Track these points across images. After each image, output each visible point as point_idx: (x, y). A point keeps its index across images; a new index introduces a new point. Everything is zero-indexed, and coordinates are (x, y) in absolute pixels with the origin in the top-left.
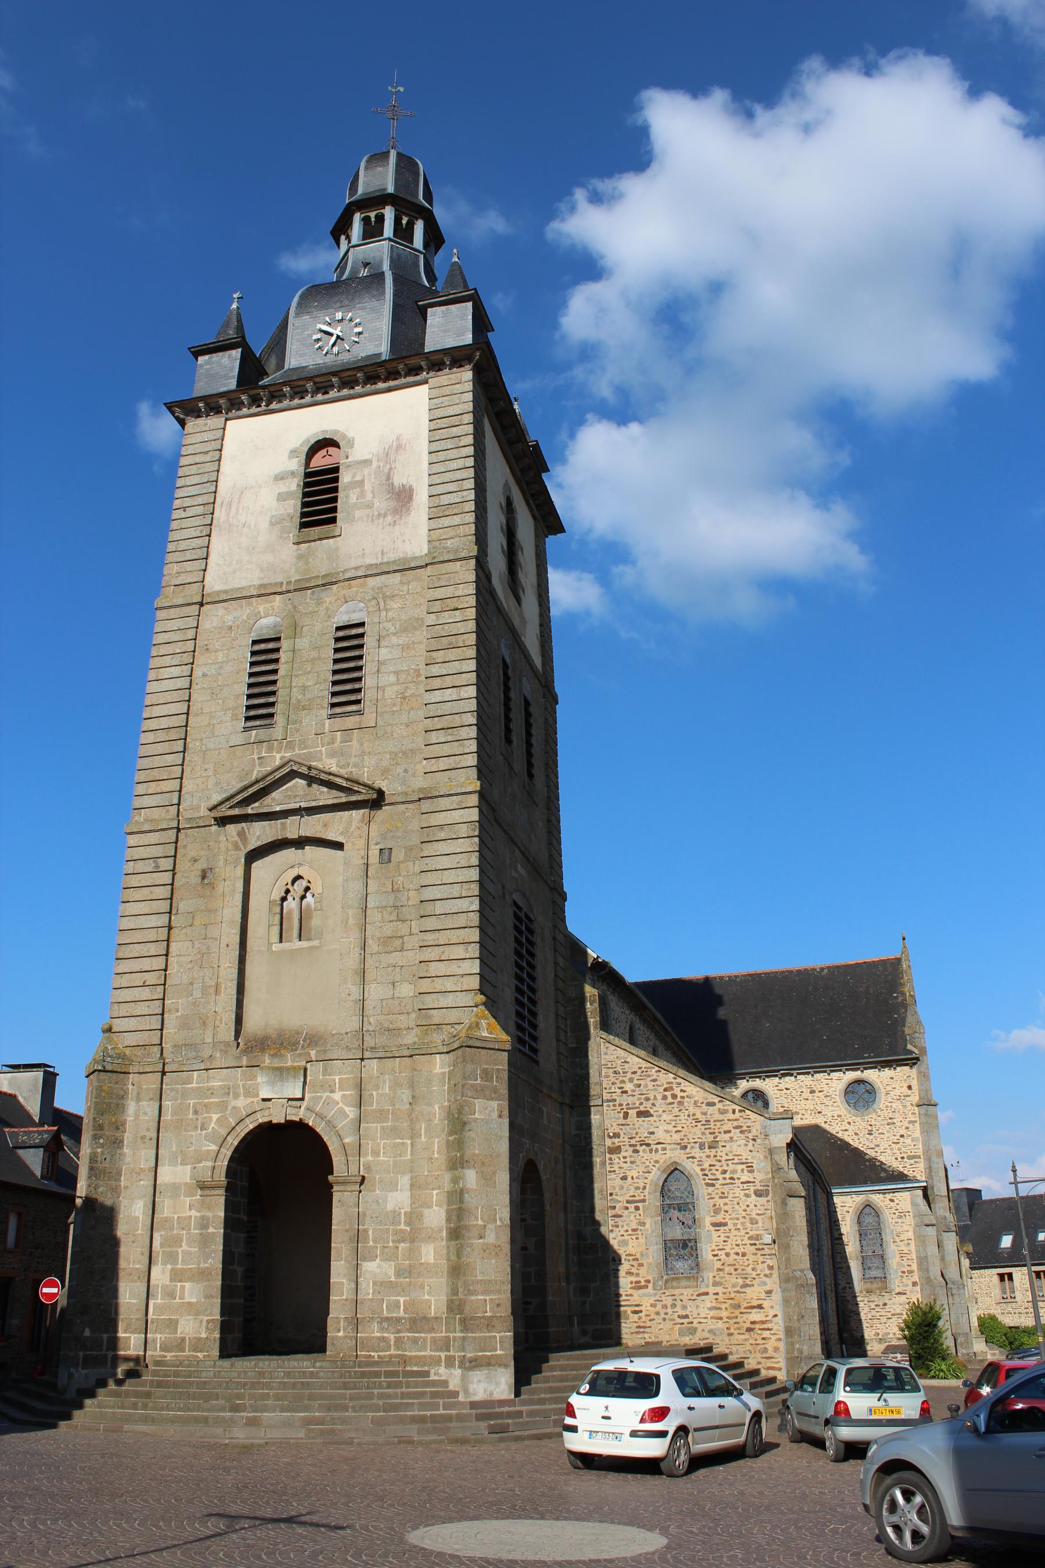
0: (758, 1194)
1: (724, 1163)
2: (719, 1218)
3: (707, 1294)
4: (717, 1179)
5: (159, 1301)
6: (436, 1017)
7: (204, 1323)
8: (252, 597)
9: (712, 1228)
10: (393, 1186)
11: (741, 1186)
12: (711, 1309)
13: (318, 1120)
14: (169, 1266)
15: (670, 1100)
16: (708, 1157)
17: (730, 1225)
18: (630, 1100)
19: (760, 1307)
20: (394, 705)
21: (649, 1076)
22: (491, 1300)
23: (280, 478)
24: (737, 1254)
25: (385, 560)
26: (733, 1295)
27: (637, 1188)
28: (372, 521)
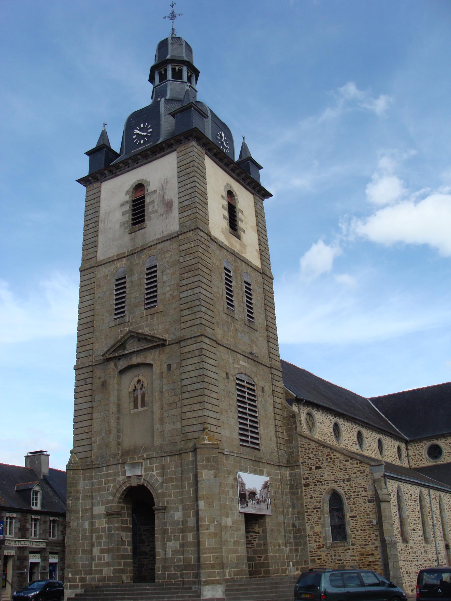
0: (370, 501)
1: (354, 488)
2: (353, 514)
3: (349, 549)
4: (351, 496)
5: (96, 562)
6: (190, 436)
7: (112, 570)
9: (350, 519)
10: (177, 509)
11: (362, 498)
12: (351, 556)
13: (148, 484)
14: (99, 548)
15: (329, 460)
16: (347, 485)
17: (358, 517)
19: (372, 554)
20: (169, 300)
21: (320, 450)
22: (213, 556)
23: (122, 205)
24: (362, 530)
25: (164, 236)
26: (360, 549)
27: (317, 502)
28: (158, 218)
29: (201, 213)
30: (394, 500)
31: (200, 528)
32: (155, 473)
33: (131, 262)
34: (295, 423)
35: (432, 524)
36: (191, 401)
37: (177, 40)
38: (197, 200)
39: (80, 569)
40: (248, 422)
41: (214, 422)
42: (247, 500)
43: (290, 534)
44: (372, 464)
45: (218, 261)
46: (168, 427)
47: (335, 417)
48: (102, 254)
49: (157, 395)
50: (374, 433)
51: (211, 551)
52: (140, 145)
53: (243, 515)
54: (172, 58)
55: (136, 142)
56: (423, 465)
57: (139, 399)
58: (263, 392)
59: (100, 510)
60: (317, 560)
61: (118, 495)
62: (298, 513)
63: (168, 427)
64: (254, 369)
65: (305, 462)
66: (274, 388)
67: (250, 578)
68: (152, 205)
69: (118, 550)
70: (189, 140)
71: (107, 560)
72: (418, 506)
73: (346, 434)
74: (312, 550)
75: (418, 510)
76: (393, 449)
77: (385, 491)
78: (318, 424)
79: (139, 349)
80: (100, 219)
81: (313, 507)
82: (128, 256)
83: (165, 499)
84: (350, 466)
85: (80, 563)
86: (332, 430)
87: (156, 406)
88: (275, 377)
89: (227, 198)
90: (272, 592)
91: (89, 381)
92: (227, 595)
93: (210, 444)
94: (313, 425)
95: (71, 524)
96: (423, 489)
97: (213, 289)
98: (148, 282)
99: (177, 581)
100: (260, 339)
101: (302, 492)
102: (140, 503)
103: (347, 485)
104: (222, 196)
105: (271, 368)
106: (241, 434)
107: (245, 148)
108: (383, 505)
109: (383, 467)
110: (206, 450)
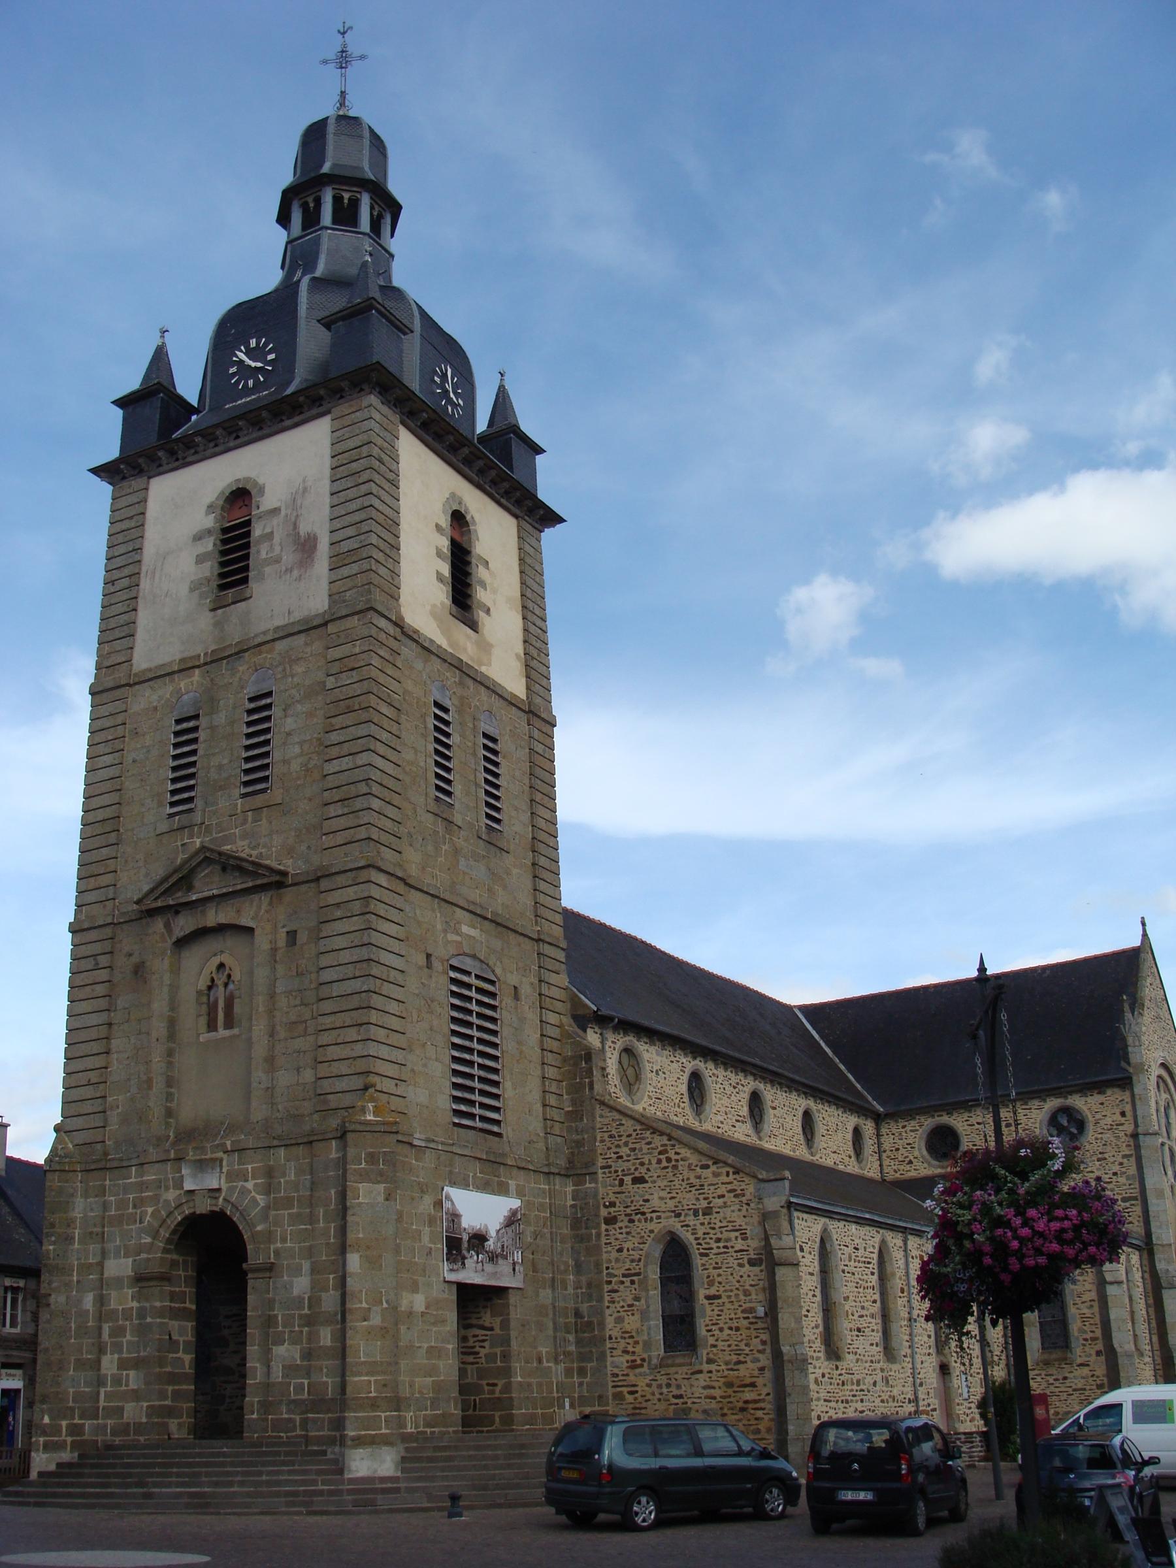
0: (752, 1263)
1: (718, 1230)
2: (712, 1291)
3: (700, 1372)
5: (109, 1389)
6: (333, 1101)
8: (173, 673)
9: (706, 1302)
10: (298, 1271)
12: (704, 1388)
14: (116, 1356)
15: (664, 1164)
16: (702, 1224)
17: (724, 1299)
18: (625, 1165)
19: (753, 1385)
20: (299, 778)
22: (376, 1381)
23: (198, 538)
24: (731, 1328)
26: (726, 1373)
27: (632, 1261)
29: (382, 571)
30: (810, 1262)
31: (349, 1317)
32: (250, 1185)
33: (212, 680)
34: (590, 1072)
35: (907, 1315)
36: (338, 1020)
37: (348, 123)
38: (374, 540)
39: (71, 1404)
40: (475, 1071)
41: (391, 1070)
42: (465, 1252)
43: (568, 1332)
44: (760, 1177)
45: (419, 685)
46: (284, 1079)
47: (695, 1058)
48: (148, 652)
49: (260, 1002)
50: (794, 1095)
51: (372, 1368)
52: (247, 391)
53: (454, 1288)
54: (336, 172)
55: (238, 382)
56: (913, 1174)
57: (220, 1010)
58: (516, 997)
59: (120, 1267)
60: (627, 1396)
61: (165, 1233)
62: (589, 1285)
63: (284, 1079)
64: (497, 944)
65: (610, 1167)
66: (545, 990)
67: (464, 1432)
68: (269, 543)
69: (161, 1362)
70: (362, 390)
71: (133, 1385)
72: (873, 1274)
73: (720, 1099)
74: (616, 1371)
75: (874, 1283)
76: (840, 1135)
77: (787, 1240)
78: (649, 1075)
79: (224, 890)
80: (144, 569)
81: (623, 1271)
82: (206, 664)
83: (272, 1247)
84: (712, 1180)
85: (71, 1390)
86: (684, 1088)
87: (259, 1029)
88: (550, 964)
89: (448, 530)
90: (509, 1466)
91: (104, 960)
92: (403, 1470)
93: (377, 1123)
94: (638, 1078)
95: (52, 1299)
96: (889, 1235)
97: (403, 755)
98: (251, 730)
99: (293, 1437)
100: (515, 871)
101: (598, 1235)
102: (213, 1251)
103: (702, 1224)
104: (437, 525)
105: (538, 940)
106: (456, 1099)
107: (504, 399)
108: (781, 1272)
109: (787, 1183)
110: (369, 1135)
